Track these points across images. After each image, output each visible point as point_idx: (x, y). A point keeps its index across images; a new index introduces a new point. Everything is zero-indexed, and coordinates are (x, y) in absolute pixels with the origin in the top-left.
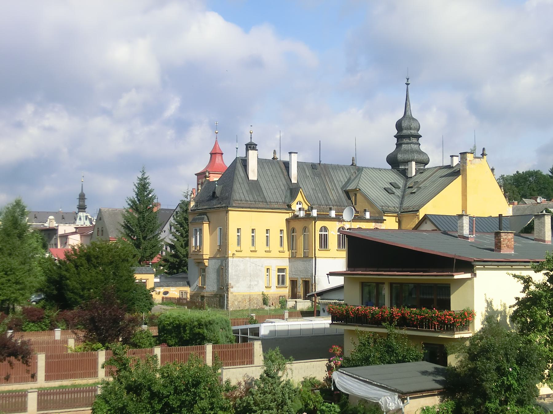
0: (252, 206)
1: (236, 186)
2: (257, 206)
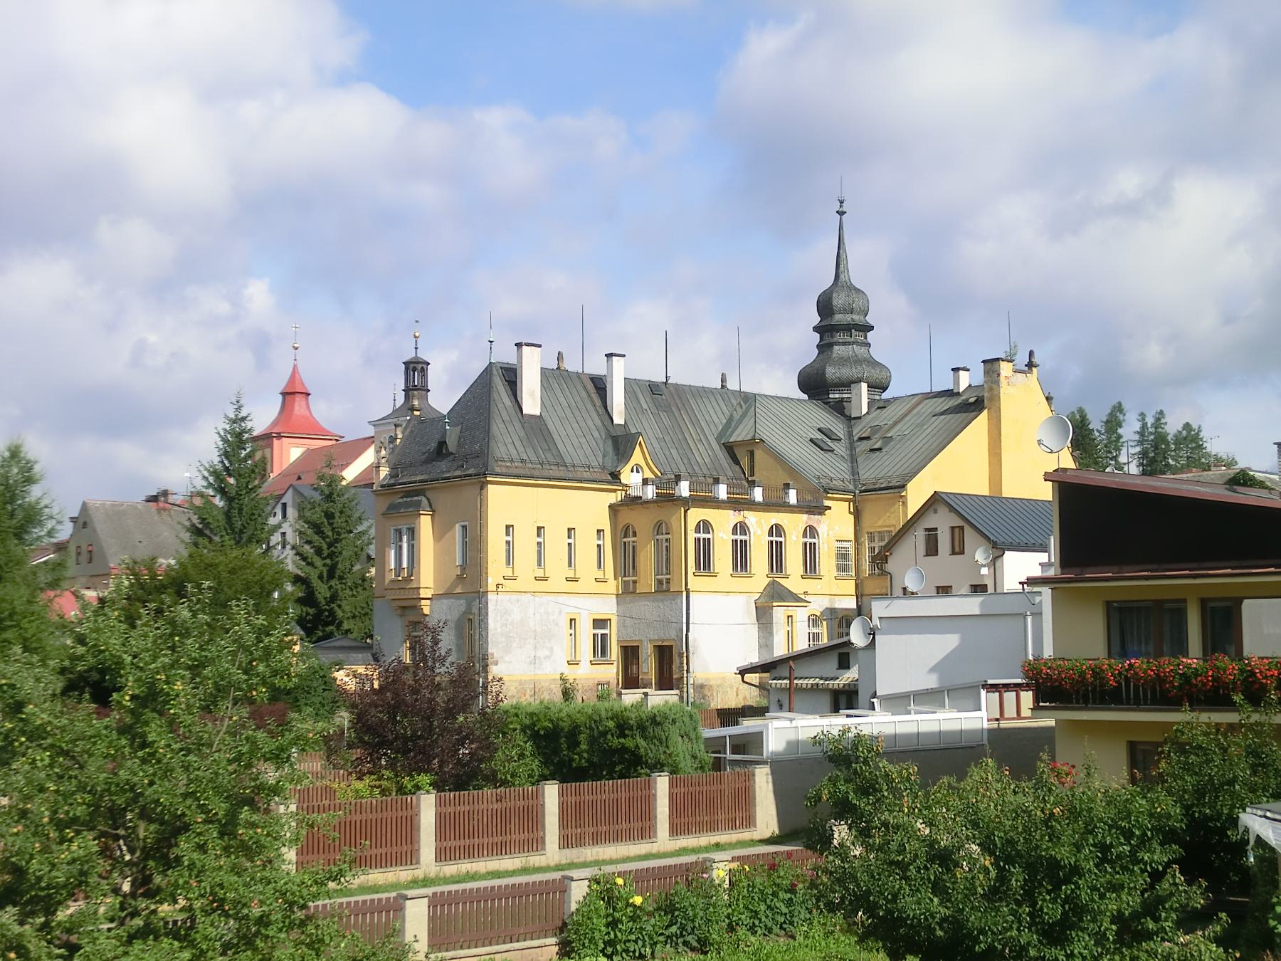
0: (536, 473)
1: (498, 428)
2: (546, 473)
